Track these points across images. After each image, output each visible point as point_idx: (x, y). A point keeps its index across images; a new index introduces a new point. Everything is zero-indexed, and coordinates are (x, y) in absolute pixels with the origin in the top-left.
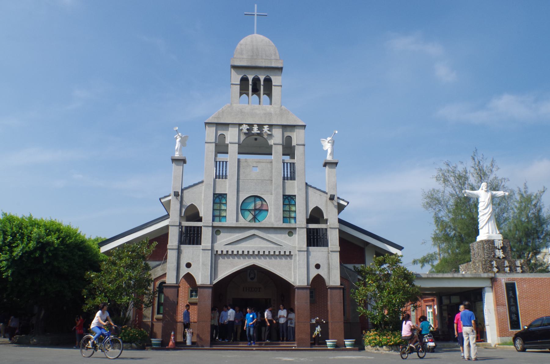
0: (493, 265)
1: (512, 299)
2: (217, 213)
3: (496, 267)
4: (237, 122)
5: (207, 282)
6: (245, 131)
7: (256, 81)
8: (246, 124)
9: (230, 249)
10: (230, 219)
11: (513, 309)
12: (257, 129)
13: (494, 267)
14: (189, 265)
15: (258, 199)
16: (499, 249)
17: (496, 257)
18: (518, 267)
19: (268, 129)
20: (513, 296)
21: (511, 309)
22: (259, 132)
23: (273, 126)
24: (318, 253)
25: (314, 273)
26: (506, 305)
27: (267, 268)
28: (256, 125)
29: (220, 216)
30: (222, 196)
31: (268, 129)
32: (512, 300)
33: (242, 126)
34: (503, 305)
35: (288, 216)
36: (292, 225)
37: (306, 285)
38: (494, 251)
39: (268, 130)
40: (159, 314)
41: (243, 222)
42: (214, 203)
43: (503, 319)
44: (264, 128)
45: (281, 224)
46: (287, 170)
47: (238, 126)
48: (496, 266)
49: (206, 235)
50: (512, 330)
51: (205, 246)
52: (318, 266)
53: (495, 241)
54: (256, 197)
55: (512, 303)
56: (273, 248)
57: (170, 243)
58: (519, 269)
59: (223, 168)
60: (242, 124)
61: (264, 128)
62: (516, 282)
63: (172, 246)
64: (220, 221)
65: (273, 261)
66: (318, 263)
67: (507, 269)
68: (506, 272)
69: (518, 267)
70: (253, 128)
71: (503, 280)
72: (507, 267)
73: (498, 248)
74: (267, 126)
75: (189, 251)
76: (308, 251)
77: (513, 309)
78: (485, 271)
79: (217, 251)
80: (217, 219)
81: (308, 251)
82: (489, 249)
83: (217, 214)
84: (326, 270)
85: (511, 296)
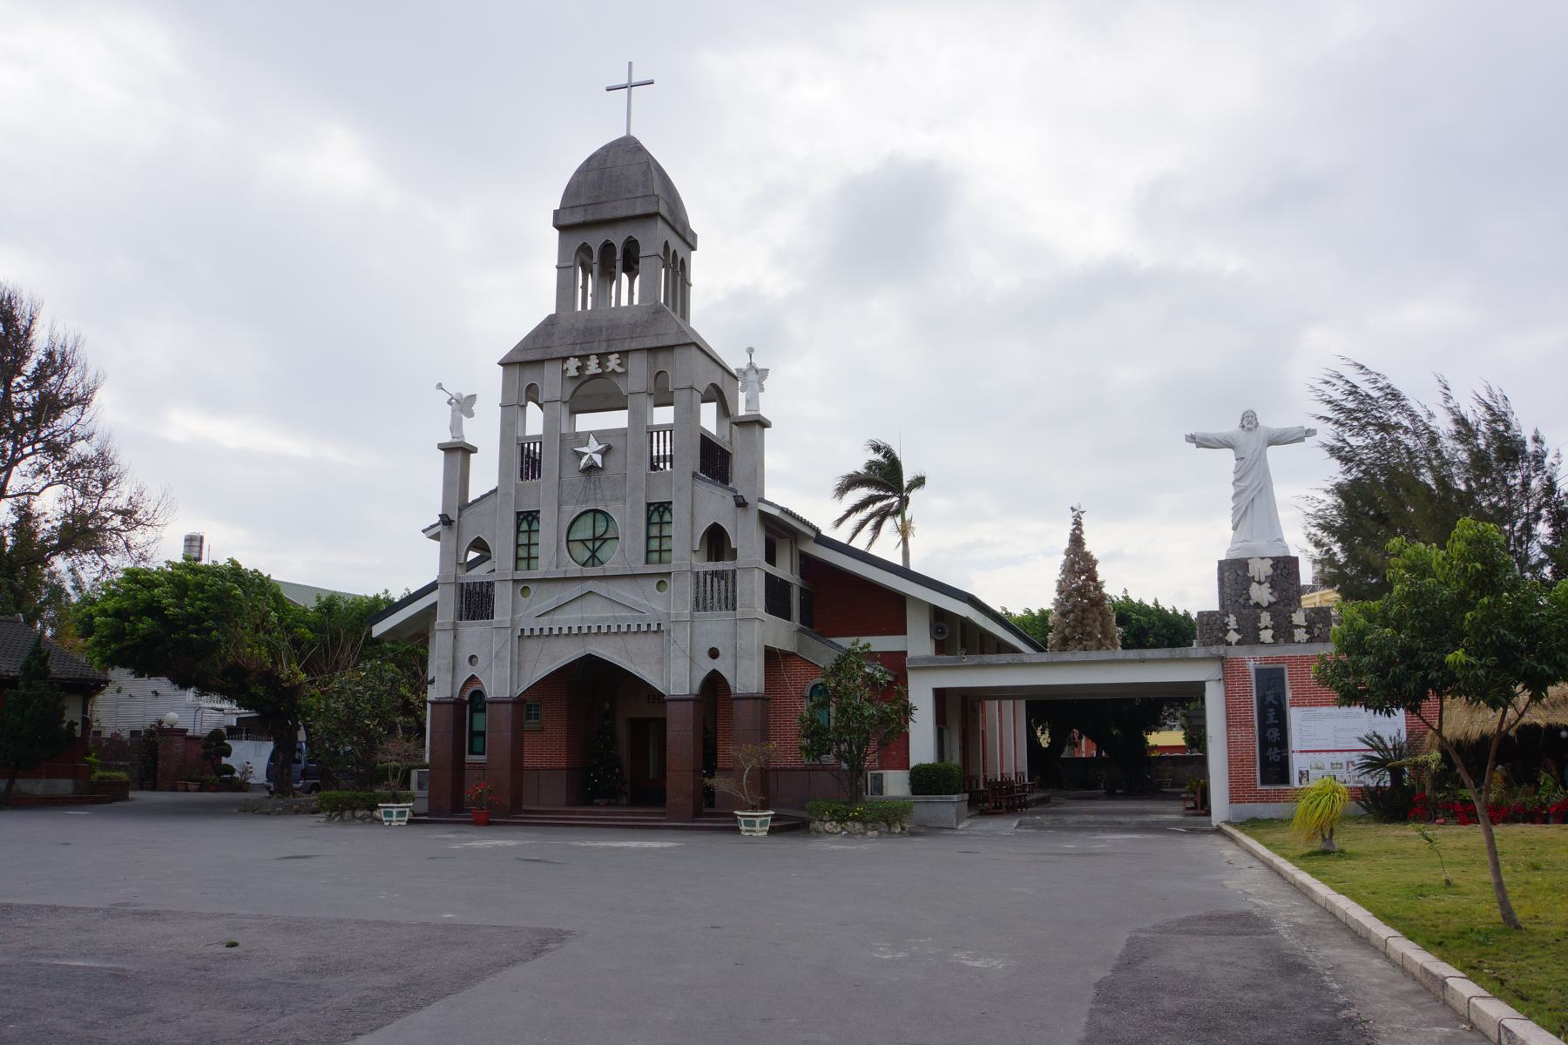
0: (1227, 624)
1: (1271, 710)
2: (523, 553)
3: (1235, 630)
4: (559, 356)
5: (506, 693)
6: (573, 372)
7: (608, 248)
8: (575, 357)
9: (545, 623)
10: (543, 568)
11: (1273, 734)
12: (597, 366)
13: (1229, 630)
14: (472, 659)
15: (599, 516)
16: (1260, 583)
17: (1252, 603)
18: (1298, 627)
19: (619, 361)
20: (1275, 702)
21: (1268, 734)
22: (600, 371)
23: (546, 363)
24: (715, 627)
25: (708, 665)
26: (1253, 726)
27: (615, 660)
28: (595, 357)
29: (529, 558)
30: (532, 515)
31: (619, 361)
32: (1271, 713)
33: (568, 362)
34: (1246, 726)
35: (656, 549)
36: (663, 569)
37: (688, 693)
38: (1247, 589)
39: (619, 365)
40: (473, 754)
41: (574, 569)
42: (649, 523)
43: (1242, 760)
44: (608, 361)
45: (640, 567)
46: (665, 446)
47: (561, 362)
48: (1236, 627)
49: (503, 598)
50: (1267, 788)
51: (501, 622)
52: (714, 654)
53: (1249, 561)
54: (596, 511)
55: (1271, 720)
56: (625, 619)
57: (741, 607)
58: (1300, 635)
59: (665, 446)
60: (568, 358)
61: (608, 361)
62: (1285, 666)
63: (443, 624)
64: (660, 561)
65: (633, 643)
66: (707, 649)
67: (1266, 635)
68: (1263, 643)
69: (1298, 627)
70: (588, 363)
71: (1252, 663)
72: (1266, 628)
73: (1257, 579)
74: (617, 356)
75: (473, 632)
76: (455, 629)
77: (1271, 734)
78: (1208, 641)
79: (522, 630)
80: (523, 564)
81: (455, 629)
82: (1237, 583)
83: (524, 555)
84: (730, 661)
85: (1271, 702)
